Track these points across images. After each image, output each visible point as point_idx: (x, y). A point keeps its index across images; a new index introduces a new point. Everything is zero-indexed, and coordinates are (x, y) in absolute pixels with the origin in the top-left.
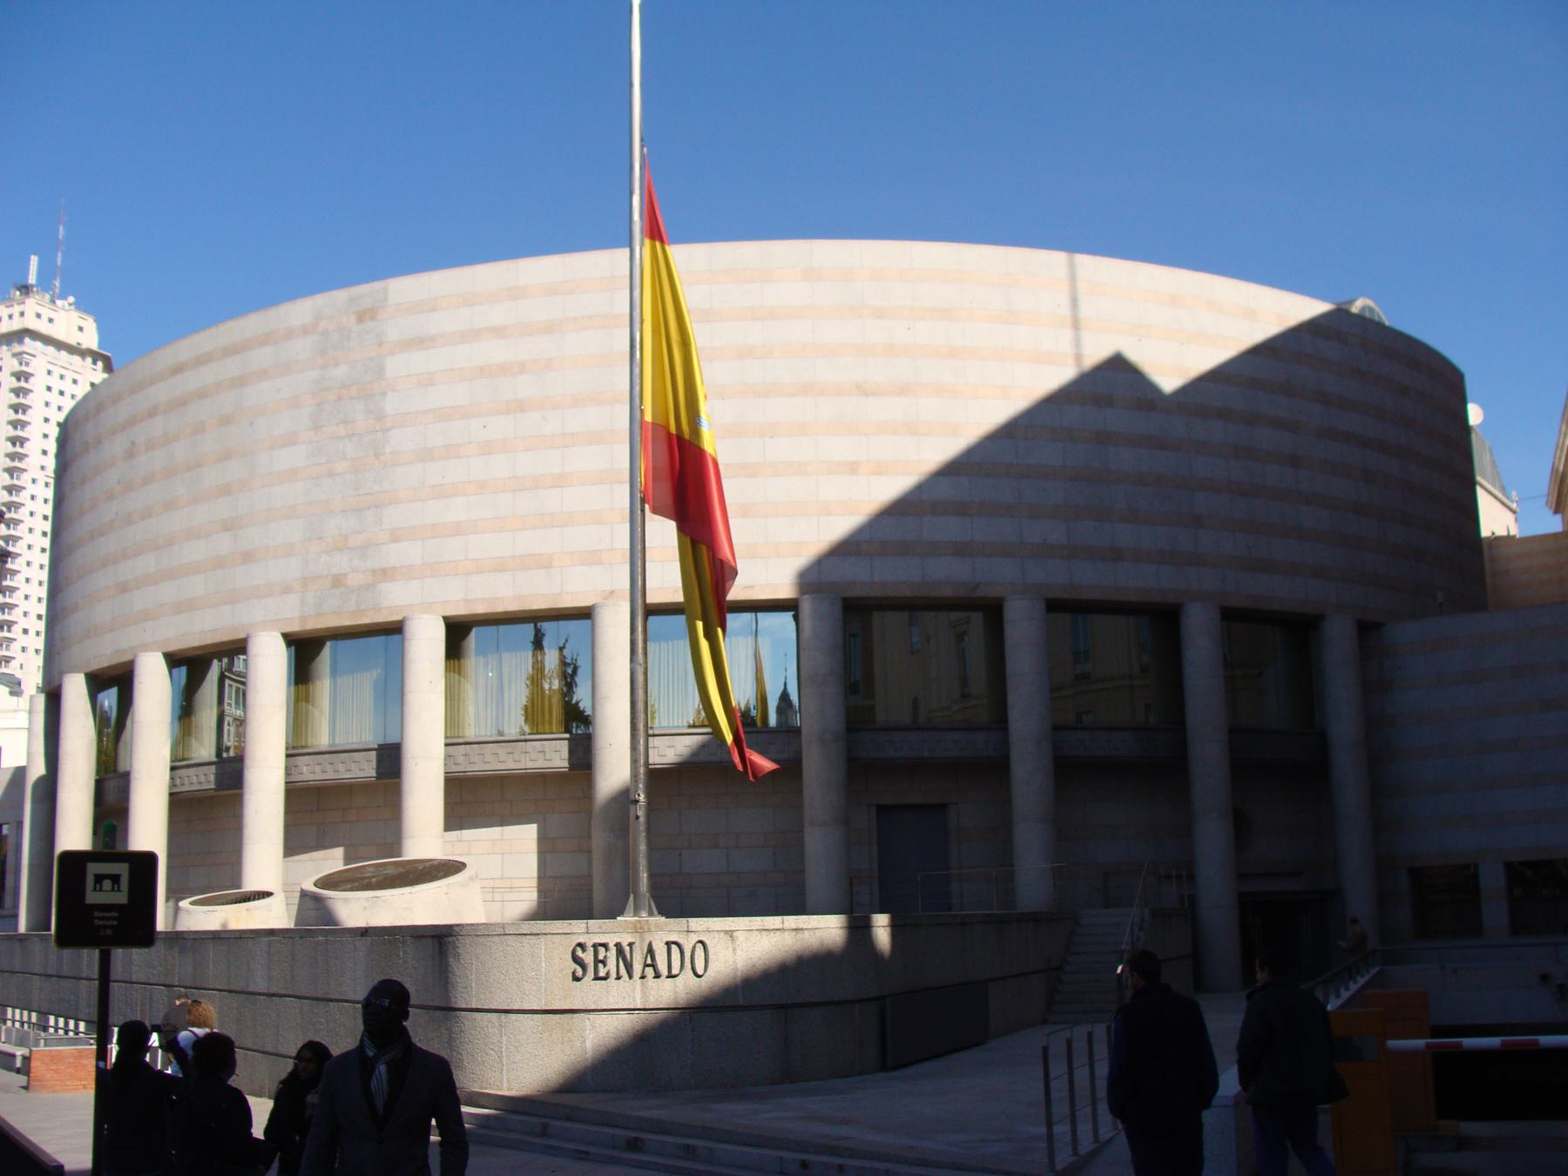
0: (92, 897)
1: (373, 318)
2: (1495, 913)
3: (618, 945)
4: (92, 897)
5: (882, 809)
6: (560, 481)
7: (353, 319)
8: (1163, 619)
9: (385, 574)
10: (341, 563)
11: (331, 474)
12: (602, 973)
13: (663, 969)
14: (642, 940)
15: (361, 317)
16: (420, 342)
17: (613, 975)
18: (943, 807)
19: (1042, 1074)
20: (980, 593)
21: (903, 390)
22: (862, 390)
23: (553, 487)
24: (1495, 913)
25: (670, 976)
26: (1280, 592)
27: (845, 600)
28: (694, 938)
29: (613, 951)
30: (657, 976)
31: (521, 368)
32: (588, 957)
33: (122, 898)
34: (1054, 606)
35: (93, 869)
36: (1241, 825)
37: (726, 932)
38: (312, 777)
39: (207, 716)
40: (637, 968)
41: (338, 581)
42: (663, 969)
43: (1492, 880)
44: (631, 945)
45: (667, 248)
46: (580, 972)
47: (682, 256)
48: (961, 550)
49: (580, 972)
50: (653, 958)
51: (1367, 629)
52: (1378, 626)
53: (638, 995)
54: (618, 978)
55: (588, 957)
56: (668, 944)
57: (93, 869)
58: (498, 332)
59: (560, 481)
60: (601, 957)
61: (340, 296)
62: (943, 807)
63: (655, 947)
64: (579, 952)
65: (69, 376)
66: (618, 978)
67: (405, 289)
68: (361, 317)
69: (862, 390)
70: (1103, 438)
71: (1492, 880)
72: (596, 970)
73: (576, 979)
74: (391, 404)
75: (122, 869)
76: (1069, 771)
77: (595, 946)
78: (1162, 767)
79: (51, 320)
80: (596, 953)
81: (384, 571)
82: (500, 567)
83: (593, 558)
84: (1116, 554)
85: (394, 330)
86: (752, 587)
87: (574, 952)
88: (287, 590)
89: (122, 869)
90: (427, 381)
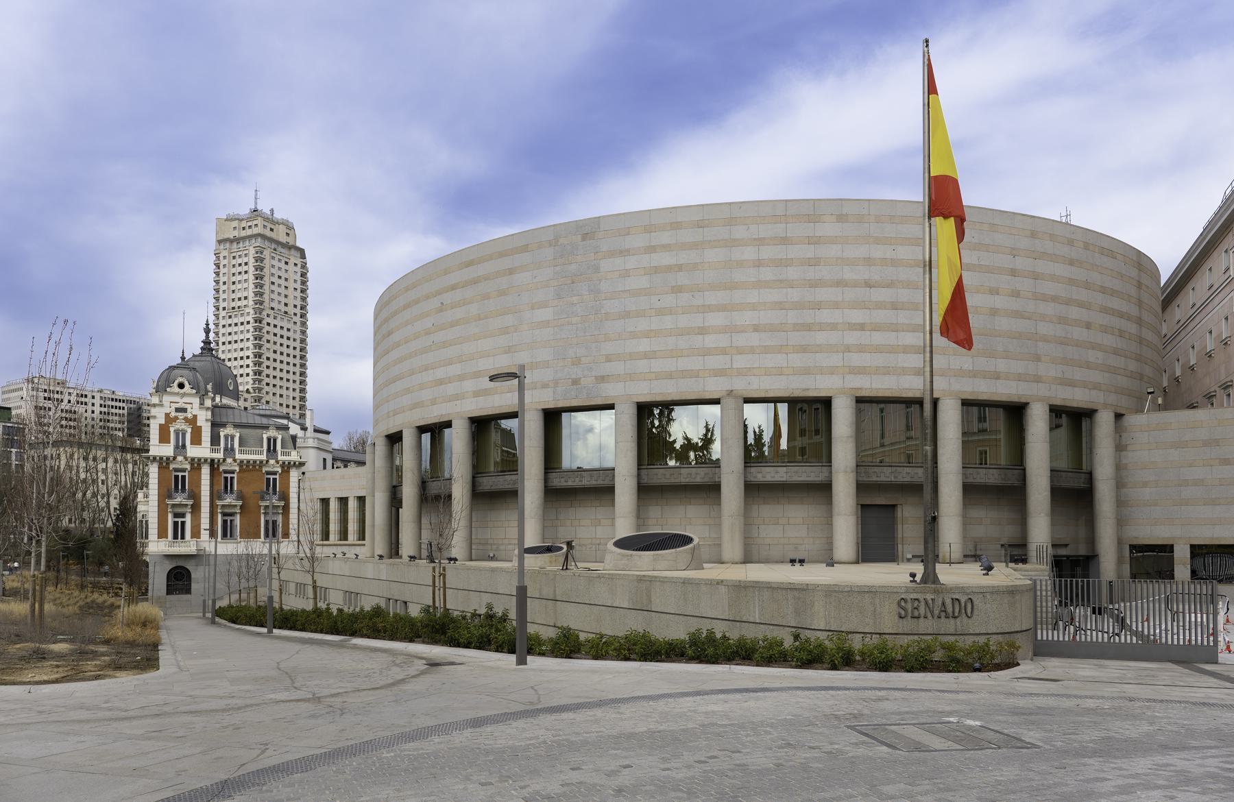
2: (1182, 571)
6: (703, 331)
7: (579, 237)
8: (1016, 412)
9: (602, 379)
18: (894, 506)
21: (891, 284)
22: (868, 284)
24: (1182, 571)
26: (1077, 398)
29: (923, 603)
31: (680, 268)
34: (966, 403)
41: (575, 382)
43: (1182, 554)
46: (903, 613)
49: (903, 613)
51: (1119, 416)
59: (703, 331)
62: (894, 506)
65: (284, 260)
69: (868, 284)
71: (1182, 554)
76: (971, 491)
78: (1013, 493)
79: (272, 230)
82: (670, 376)
84: (997, 376)
88: (545, 386)
90: (626, 274)
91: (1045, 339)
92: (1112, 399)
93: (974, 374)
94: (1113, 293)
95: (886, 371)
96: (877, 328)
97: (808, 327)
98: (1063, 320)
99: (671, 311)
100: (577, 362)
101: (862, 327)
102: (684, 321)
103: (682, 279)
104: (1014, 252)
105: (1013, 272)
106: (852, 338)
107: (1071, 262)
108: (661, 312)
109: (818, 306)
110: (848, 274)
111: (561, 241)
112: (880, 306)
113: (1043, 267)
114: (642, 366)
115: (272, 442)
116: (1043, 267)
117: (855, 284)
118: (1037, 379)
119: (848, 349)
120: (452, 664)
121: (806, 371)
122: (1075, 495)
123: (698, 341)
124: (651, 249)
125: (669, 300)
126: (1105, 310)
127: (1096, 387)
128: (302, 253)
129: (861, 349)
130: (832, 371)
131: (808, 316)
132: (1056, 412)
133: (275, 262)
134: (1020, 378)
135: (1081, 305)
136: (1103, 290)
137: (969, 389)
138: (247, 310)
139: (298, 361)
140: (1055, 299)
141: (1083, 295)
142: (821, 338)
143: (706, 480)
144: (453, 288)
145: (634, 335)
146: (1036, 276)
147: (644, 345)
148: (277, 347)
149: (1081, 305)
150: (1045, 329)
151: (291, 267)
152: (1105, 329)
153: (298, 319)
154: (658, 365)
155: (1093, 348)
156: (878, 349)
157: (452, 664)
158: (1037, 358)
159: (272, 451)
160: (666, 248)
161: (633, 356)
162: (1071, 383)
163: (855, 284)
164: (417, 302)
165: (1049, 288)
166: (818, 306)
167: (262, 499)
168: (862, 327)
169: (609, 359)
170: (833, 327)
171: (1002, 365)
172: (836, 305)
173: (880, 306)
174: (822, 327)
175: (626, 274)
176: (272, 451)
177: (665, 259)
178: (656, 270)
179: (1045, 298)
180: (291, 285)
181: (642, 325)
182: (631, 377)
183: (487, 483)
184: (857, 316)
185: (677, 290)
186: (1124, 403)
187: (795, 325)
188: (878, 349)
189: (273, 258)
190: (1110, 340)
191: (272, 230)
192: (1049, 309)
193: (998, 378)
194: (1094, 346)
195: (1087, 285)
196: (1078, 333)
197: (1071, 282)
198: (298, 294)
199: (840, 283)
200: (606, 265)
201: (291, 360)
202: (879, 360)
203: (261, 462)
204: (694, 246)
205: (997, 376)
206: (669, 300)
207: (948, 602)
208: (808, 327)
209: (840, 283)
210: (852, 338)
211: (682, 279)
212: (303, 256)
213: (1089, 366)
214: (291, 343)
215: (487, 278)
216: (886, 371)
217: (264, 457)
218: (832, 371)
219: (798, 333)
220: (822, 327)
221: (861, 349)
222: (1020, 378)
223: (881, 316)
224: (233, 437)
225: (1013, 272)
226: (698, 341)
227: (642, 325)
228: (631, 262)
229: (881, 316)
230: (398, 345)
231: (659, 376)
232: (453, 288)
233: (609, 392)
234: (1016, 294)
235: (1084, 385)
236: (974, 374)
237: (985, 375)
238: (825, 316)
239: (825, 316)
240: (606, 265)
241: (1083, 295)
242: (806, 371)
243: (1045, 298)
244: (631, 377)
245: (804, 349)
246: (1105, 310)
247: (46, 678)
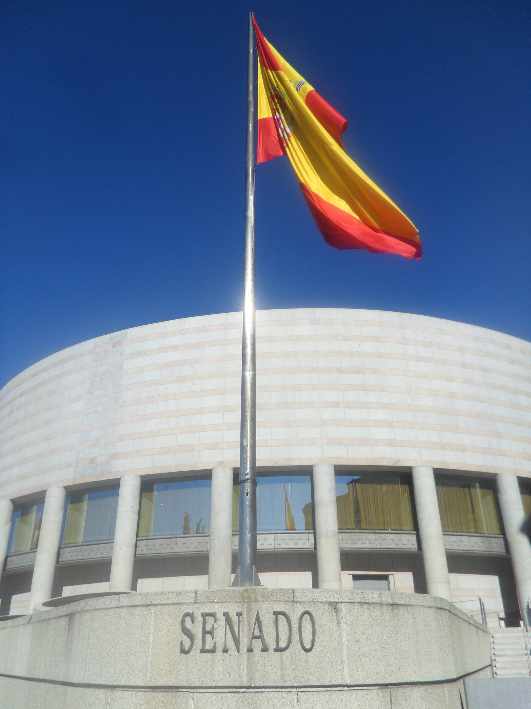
3: (226, 614)
6: (200, 412)
9: (115, 456)
12: (208, 646)
13: (272, 645)
14: (249, 611)
15: (114, 346)
16: (141, 354)
17: (220, 649)
19: (140, 685)
21: (358, 371)
22: (339, 371)
23: (196, 414)
25: (278, 650)
27: (336, 467)
28: (300, 609)
29: (222, 619)
30: (265, 649)
32: (197, 630)
37: (330, 604)
38: (71, 559)
39: (35, 537)
40: (244, 641)
41: (92, 461)
42: (272, 645)
44: (239, 614)
48: (390, 443)
50: (261, 630)
53: (244, 671)
54: (225, 651)
55: (197, 630)
56: (276, 614)
58: (174, 348)
60: (208, 628)
63: (262, 618)
64: (188, 624)
66: (225, 651)
68: (114, 346)
69: (339, 371)
70: (452, 395)
72: (204, 623)
73: (184, 651)
77: (205, 615)
80: (204, 623)
81: (115, 455)
84: (464, 449)
86: (290, 459)
87: (183, 622)
96: (349, 405)
101: (337, 405)
105: (464, 365)
107: (513, 362)
143: (200, 549)
146: (485, 370)
168: (337, 405)
205: (464, 449)
207: (267, 619)
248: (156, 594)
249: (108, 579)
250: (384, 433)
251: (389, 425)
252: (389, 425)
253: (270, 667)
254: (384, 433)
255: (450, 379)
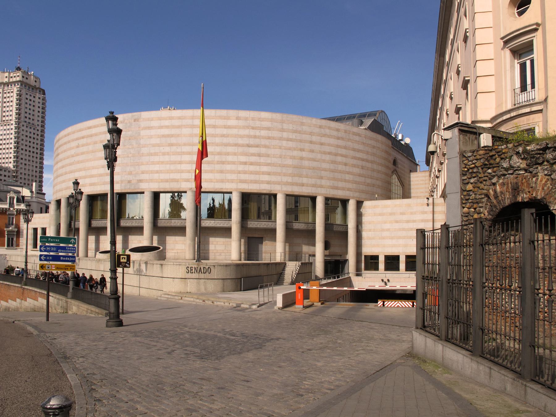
0: (121, 261)
1: (138, 121)
4: (121, 261)
5: (248, 237)
6: (180, 163)
7: (133, 120)
9: (140, 181)
10: (130, 178)
11: (128, 157)
15: (135, 120)
18: (262, 238)
20: (272, 192)
21: (257, 146)
22: (249, 146)
26: (340, 194)
33: (126, 261)
35: (122, 257)
36: (327, 246)
41: (129, 182)
43: (382, 259)
45: (205, 110)
47: (207, 112)
48: (268, 183)
51: (359, 204)
52: (362, 202)
57: (122, 257)
58: (167, 127)
59: (180, 163)
61: (129, 115)
62: (262, 238)
67: (145, 115)
68: (135, 120)
69: (249, 146)
70: (302, 158)
71: (382, 259)
74: (142, 142)
75: (126, 257)
79: (27, 78)
82: (167, 181)
83: (187, 180)
84: (303, 185)
85: (143, 124)
89: (126, 257)
90: (151, 137)
91: (325, 170)
92: (357, 195)
93: (292, 184)
94: (359, 151)
95: (256, 182)
96: (252, 164)
97: (223, 163)
98: (334, 162)
99: (168, 154)
100: (130, 173)
101: (245, 163)
102: (174, 158)
103: (173, 140)
104: (311, 134)
105: (311, 142)
106: (241, 168)
107: (338, 138)
108: (164, 154)
109: (228, 154)
110: (240, 141)
111: (126, 121)
112: (253, 155)
113: (324, 140)
114: (156, 176)
115: (12, 199)
116: (324, 140)
117: (243, 146)
118: (321, 186)
119: (239, 172)
120: (204, 144)
121: (222, 181)
122: (336, 235)
123: (179, 167)
124: (161, 127)
125: (167, 149)
126: (354, 158)
127: (349, 190)
128: (44, 91)
129: (245, 172)
130: (232, 181)
131: (224, 158)
132: (327, 199)
133: (28, 97)
134: (314, 186)
135: (342, 155)
136: (354, 150)
137: (290, 190)
138: (12, 122)
139: (39, 151)
140: (330, 153)
141: (344, 152)
142: (228, 167)
144: (83, 138)
145: (153, 163)
146: (322, 144)
147: (156, 168)
148: (28, 143)
149: (342, 155)
150: (325, 165)
151: (37, 100)
152: (354, 166)
153: (39, 128)
154: (163, 176)
155: (348, 174)
156: (251, 173)
157: (204, 144)
158: (321, 178)
159: (11, 204)
160: (167, 127)
161: (152, 172)
162: (337, 188)
163: (243, 146)
164: (69, 142)
165: (327, 149)
166: (228, 154)
167: (7, 227)
168: (245, 163)
169: (143, 173)
170: (233, 163)
171: (305, 180)
172: (235, 154)
173: (253, 155)
174: (229, 163)
175: (151, 137)
176: (11, 204)
177: (166, 132)
178: (163, 136)
179: (325, 153)
180: (37, 109)
181: (156, 159)
182: (151, 181)
183: (95, 223)
184: (243, 159)
185: (171, 145)
186: (361, 197)
187: (218, 161)
188: (251, 173)
189: (27, 94)
190: (357, 170)
191: (27, 78)
192: (328, 157)
193: (303, 186)
194: (349, 173)
195: (345, 148)
196: (340, 167)
197: (338, 146)
198: (40, 114)
199: (236, 145)
200: (143, 133)
201: (35, 150)
202: (252, 177)
203: (6, 209)
204: (179, 127)
205: (303, 185)
206: (167, 149)
208: (223, 163)
209: (236, 145)
210: (241, 168)
211: (173, 140)
212: (44, 94)
213: (345, 181)
214: (35, 141)
215: (96, 135)
216: (252, 182)
217: (7, 206)
218: (232, 181)
219: (219, 165)
220: (229, 163)
221: (245, 172)
222: (314, 186)
223: (253, 159)
224: (13, 198)
225: (311, 142)
226: (179, 167)
227: (156, 159)
228: (153, 132)
229: (253, 159)
230: (61, 160)
231: (163, 181)
232: (83, 138)
233: (143, 186)
234: (312, 151)
235: (343, 189)
236: (292, 184)
237: (297, 184)
238: (230, 158)
239: (230, 158)
240: (143, 133)
241: (344, 152)
242: (222, 181)
243: (325, 153)
244: (151, 181)
245: (221, 172)
246: (354, 158)
247: (257, 236)
248: (467, 357)
249: (406, 270)
250: (266, 178)
251: (269, 174)
252: (269, 174)
253: (202, 276)
254: (266, 178)
255: (302, 150)
